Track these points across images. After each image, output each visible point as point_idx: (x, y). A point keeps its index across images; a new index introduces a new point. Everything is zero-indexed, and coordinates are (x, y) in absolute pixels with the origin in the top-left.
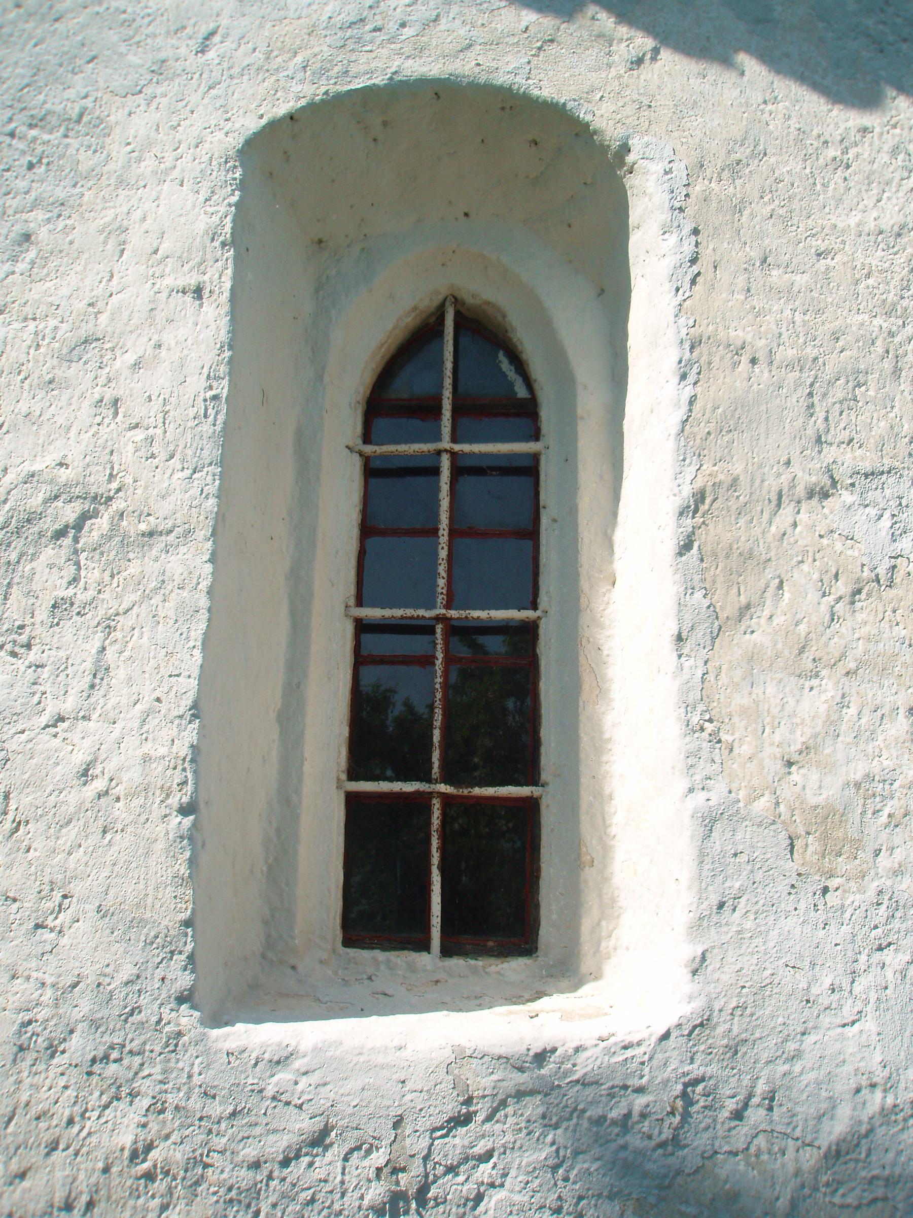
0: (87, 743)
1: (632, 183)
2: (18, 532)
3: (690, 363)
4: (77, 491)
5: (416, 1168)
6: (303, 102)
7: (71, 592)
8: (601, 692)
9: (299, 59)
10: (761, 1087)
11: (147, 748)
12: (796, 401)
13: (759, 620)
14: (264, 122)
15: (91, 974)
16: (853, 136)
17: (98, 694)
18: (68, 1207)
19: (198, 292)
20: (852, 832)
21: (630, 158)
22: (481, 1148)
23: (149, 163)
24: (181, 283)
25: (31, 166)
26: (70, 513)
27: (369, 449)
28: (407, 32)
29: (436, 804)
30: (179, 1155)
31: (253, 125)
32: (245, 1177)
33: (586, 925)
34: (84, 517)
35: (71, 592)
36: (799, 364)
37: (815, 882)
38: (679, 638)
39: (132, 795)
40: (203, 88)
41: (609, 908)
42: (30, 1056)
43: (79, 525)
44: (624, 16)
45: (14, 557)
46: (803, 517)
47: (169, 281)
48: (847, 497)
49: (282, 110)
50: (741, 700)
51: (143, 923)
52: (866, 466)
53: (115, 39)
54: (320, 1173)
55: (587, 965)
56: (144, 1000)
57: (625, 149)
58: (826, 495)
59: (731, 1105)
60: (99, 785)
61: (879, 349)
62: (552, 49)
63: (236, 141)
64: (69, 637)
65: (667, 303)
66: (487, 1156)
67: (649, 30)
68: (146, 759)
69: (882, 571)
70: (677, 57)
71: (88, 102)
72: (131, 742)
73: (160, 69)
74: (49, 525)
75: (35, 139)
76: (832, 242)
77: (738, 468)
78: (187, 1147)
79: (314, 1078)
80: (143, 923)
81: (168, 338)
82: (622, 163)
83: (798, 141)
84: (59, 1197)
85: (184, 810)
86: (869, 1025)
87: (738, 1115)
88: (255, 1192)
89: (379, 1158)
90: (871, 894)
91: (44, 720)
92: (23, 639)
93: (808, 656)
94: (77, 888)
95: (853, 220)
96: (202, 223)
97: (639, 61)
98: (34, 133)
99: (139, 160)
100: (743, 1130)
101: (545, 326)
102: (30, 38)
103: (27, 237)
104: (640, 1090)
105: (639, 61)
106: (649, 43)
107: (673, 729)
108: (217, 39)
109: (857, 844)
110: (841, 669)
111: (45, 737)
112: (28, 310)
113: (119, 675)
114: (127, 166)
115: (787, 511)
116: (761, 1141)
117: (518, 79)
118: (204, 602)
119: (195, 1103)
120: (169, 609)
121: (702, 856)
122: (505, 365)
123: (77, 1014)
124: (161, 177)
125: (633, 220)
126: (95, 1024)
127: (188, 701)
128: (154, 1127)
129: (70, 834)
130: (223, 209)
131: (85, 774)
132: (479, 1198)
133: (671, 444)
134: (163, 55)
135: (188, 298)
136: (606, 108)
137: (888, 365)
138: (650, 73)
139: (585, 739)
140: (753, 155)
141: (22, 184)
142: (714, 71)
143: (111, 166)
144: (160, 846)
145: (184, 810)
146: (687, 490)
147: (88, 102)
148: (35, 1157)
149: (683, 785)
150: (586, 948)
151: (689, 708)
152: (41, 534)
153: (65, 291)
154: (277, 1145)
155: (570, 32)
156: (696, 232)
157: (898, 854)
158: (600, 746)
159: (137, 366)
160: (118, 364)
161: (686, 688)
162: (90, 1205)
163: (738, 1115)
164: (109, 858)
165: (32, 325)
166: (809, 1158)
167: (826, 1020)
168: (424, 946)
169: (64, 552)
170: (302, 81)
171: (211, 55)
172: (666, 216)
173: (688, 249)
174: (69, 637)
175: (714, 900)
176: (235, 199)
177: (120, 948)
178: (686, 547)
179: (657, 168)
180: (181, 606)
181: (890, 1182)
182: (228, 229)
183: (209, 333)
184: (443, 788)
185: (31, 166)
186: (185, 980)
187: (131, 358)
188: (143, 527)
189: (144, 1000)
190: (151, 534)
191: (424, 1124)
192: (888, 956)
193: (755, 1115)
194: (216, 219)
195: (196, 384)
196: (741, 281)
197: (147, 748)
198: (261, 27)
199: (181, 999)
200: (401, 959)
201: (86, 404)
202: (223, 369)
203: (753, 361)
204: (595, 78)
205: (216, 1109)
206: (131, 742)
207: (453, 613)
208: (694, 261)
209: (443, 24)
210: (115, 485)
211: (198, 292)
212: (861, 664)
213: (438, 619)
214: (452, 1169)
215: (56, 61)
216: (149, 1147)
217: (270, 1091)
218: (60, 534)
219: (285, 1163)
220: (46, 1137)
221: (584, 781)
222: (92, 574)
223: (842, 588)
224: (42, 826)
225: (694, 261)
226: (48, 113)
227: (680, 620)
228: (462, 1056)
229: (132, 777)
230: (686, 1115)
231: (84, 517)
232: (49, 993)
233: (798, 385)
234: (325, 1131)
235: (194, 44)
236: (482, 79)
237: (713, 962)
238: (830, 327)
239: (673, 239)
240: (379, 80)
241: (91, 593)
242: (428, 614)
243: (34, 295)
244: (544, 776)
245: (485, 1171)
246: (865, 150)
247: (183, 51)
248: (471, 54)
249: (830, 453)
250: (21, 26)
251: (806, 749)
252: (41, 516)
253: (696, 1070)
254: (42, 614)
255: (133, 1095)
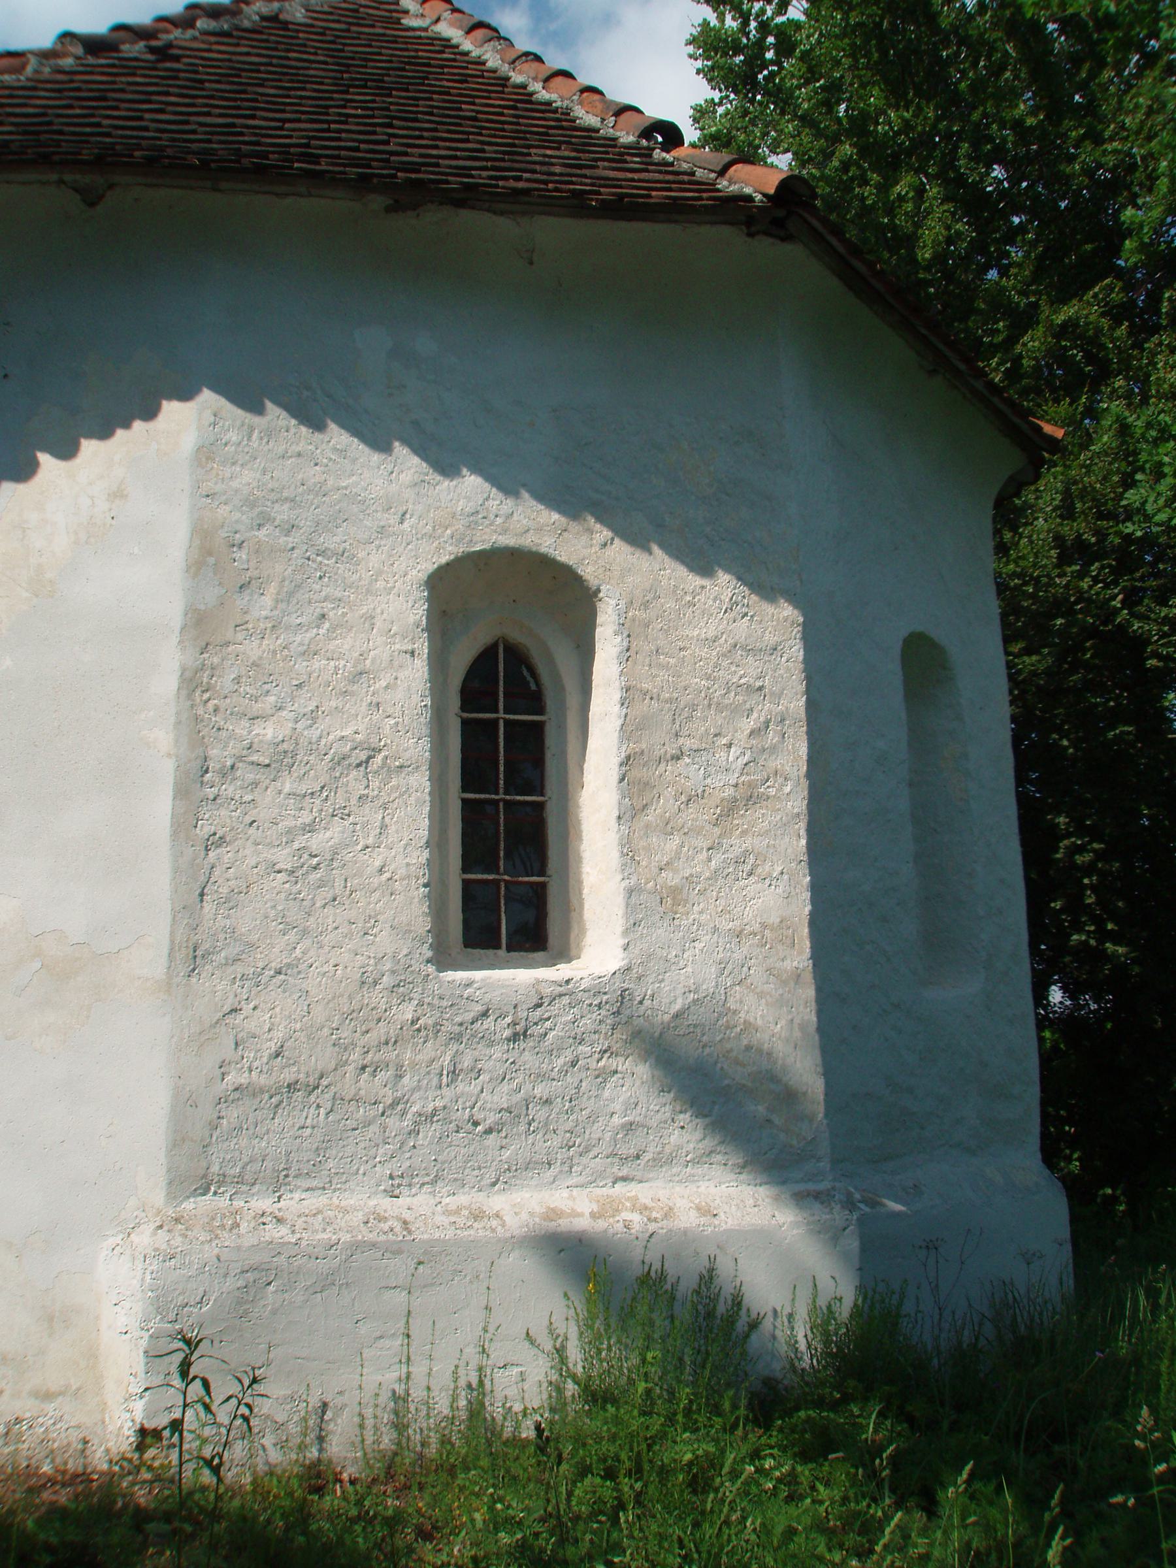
0: (380, 857)
1: (600, 606)
2: (339, 763)
3: (625, 699)
4: (366, 746)
5: (523, 1023)
6: (452, 557)
7: (366, 792)
8: (579, 838)
9: (449, 532)
10: (649, 992)
11: (408, 860)
12: (668, 717)
13: (651, 810)
14: (436, 566)
15: (390, 951)
16: (698, 590)
17: (383, 837)
18: (387, 1043)
19: (412, 653)
20: (684, 897)
21: (601, 595)
22: (547, 1015)
23: (380, 584)
24: (404, 648)
25: (321, 578)
26: (363, 756)
27: (466, 715)
28: (499, 520)
29: (503, 885)
30: (430, 1022)
31: (431, 568)
32: (457, 1029)
33: (572, 936)
34: (370, 758)
35: (366, 792)
36: (670, 701)
37: (670, 915)
38: (619, 818)
39: (402, 879)
40: (404, 544)
41: (583, 931)
42: (367, 986)
43: (367, 762)
44: (599, 519)
45: (338, 774)
46: (669, 768)
47: (397, 646)
48: (687, 760)
49: (444, 560)
50: (643, 843)
51: (410, 931)
52: (695, 747)
53: (356, 510)
54: (485, 1027)
55: (573, 952)
56: (413, 962)
57: (599, 591)
58: (678, 759)
59: (638, 999)
60: (387, 875)
61: (703, 695)
62: (565, 534)
63: (423, 576)
64: (367, 811)
65: (615, 669)
66: (548, 1019)
67: (610, 527)
68: (408, 865)
69: (699, 791)
70: (622, 543)
71: (347, 545)
72: (399, 858)
73: (382, 531)
74: (354, 760)
75: (321, 563)
76: (686, 644)
77: (644, 746)
78: (433, 1019)
79: (483, 991)
80: (410, 931)
81: (401, 675)
82: (596, 596)
83: (674, 592)
84: (383, 1039)
85: (425, 886)
86: (689, 969)
87: (641, 1002)
88: (461, 1034)
89: (509, 1020)
90: (691, 920)
91: (359, 847)
92: (346, 812)
93: (669, 826)
94: (381, 918)
95: (696, 633)
96: (412, 619)
97: (605, 545)
98: (319, 559)
99: (376, 581)
100: (643, 1008)
101: (552, 662)
102: (312, 504)
103: (323, 616)
104: (605, 993)
105: (605, 545)
106: (610, 534)
107: (615, 854)
108: (408, 516)
109: (686, 901)
110: (682, 832)
111: (360, 855)
112: (329, 655)
113: (392, 829)
114: (370, 583)
115: (663, 765)
116: (649, 1012)
117: (551, 551)
118: (428, 798)
119: (436, 1001)
120: (412, 800)
121: (627, 905)
122: (525, 672)
123: (386, 968)
124: (389, 591)
125: (599, 620)
126: (393, 972)
127: (424, 840)
128: (420, 1011)
129: (377, 894)
130: (421, 612)
131: (381, 871)
132: (546, 1034)
133: (617, 734)
134: (382, 524)
135: (408, 656)
136: (590, 569)
137: (706, 702)
138: (611, 551)
139: (571, 857)
140: (654, 598)
141: (317, 587)
142: (638, 553)
143: (363, 583)
144: (416, 900)
145: (425, 886)
146: (623, 755)
147: (347, 545)
148: (372, 1024)
149: (620, 877)
150: (573, 946)
151: (623, 846)
152: (350, 765)
153: (346, 647)
154: (469, 1017)
155: (574, 526)
156: (629, 636)
157: (701, 905)
158: (579, 860)
159: (387, 687)
160: (377, 685)
161: (621, 839)
162: (396, 1042)
163: (641, 1002)
164: (394, 906)
165: (332, 663)
166: (667, 1018)
167: (673, 968)
168: (498, 946)
169: (362, 774)
170: (451, 544)
171: (406, 525)
172: (616, 627)
173: (625, 644)
174: (367, 811)
175: (632, 922)
176: (426, 607)
177: (402, 942)
178: (622, 780)
179: (613, 602)
180: (417, 800)
181: (695, 1026)
182: (424, 622)
183: (420, 673)
184: (506, 877)
185: (321, 578)
186: (429, 954)
187: (383, 683)
188: (397, 764)
189: (413, 962)
190: (401, 767)
191: (525, 1007)
192: (696, 944)
193: (647, 1003)
194: (418, 617)
195: (416, 698)
196: (647, 661)
197: (408, 860)
198: (429, 511)
199: (428, 961)
200: (490, 952)
201: (364, 704)
202: (427, 692)
203: (652, 698)
204: (586, 552)
205: (445, 1003)
206: (399, 858)
207: (508, 797)
208: (628, 650)
209: (515, 517)
210: (382, 743)
211: (412, 653)
212: (690, 830)
213: (501, 800)
214: (536, 1024)
215: (327, 519)
216: (418, 1019)
217: (465, 996)
218: (359, 765)
219: (472, 1023)
220: (376, 1017)
221: (571, 875)
222: (375, 783)
223: (683, 798)
224: (363, 893)
225: (628, 650)
226: (326, 549)
227: (619, 810)
228: (538, 982)
229: (402, 872)
230: (622, 1003)
231: (370, 758)
232: (372, 961)
233: (670, 710)
234: (488, 1010)
235: (398, 517)
236: (534, 549)
237: (631, 947)
238: (683, 684)
239: (619, 639)
240: (487, 546)
241: (376, 793)
242: (497, 797)
243: (331, 647)
244: (549, 872)
245: (548, 1024)
246: (702, 597)
247: (392, 522)
248: (529, 535)
249: (681, 741)
250: (306, 497)
251: (668, 864)
252: (349, 756)
253: (626, 985)
254: (354, 801)
255: (410, 999)
